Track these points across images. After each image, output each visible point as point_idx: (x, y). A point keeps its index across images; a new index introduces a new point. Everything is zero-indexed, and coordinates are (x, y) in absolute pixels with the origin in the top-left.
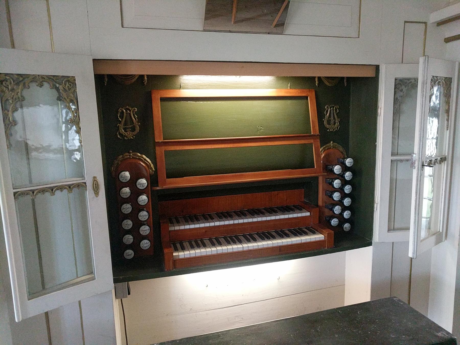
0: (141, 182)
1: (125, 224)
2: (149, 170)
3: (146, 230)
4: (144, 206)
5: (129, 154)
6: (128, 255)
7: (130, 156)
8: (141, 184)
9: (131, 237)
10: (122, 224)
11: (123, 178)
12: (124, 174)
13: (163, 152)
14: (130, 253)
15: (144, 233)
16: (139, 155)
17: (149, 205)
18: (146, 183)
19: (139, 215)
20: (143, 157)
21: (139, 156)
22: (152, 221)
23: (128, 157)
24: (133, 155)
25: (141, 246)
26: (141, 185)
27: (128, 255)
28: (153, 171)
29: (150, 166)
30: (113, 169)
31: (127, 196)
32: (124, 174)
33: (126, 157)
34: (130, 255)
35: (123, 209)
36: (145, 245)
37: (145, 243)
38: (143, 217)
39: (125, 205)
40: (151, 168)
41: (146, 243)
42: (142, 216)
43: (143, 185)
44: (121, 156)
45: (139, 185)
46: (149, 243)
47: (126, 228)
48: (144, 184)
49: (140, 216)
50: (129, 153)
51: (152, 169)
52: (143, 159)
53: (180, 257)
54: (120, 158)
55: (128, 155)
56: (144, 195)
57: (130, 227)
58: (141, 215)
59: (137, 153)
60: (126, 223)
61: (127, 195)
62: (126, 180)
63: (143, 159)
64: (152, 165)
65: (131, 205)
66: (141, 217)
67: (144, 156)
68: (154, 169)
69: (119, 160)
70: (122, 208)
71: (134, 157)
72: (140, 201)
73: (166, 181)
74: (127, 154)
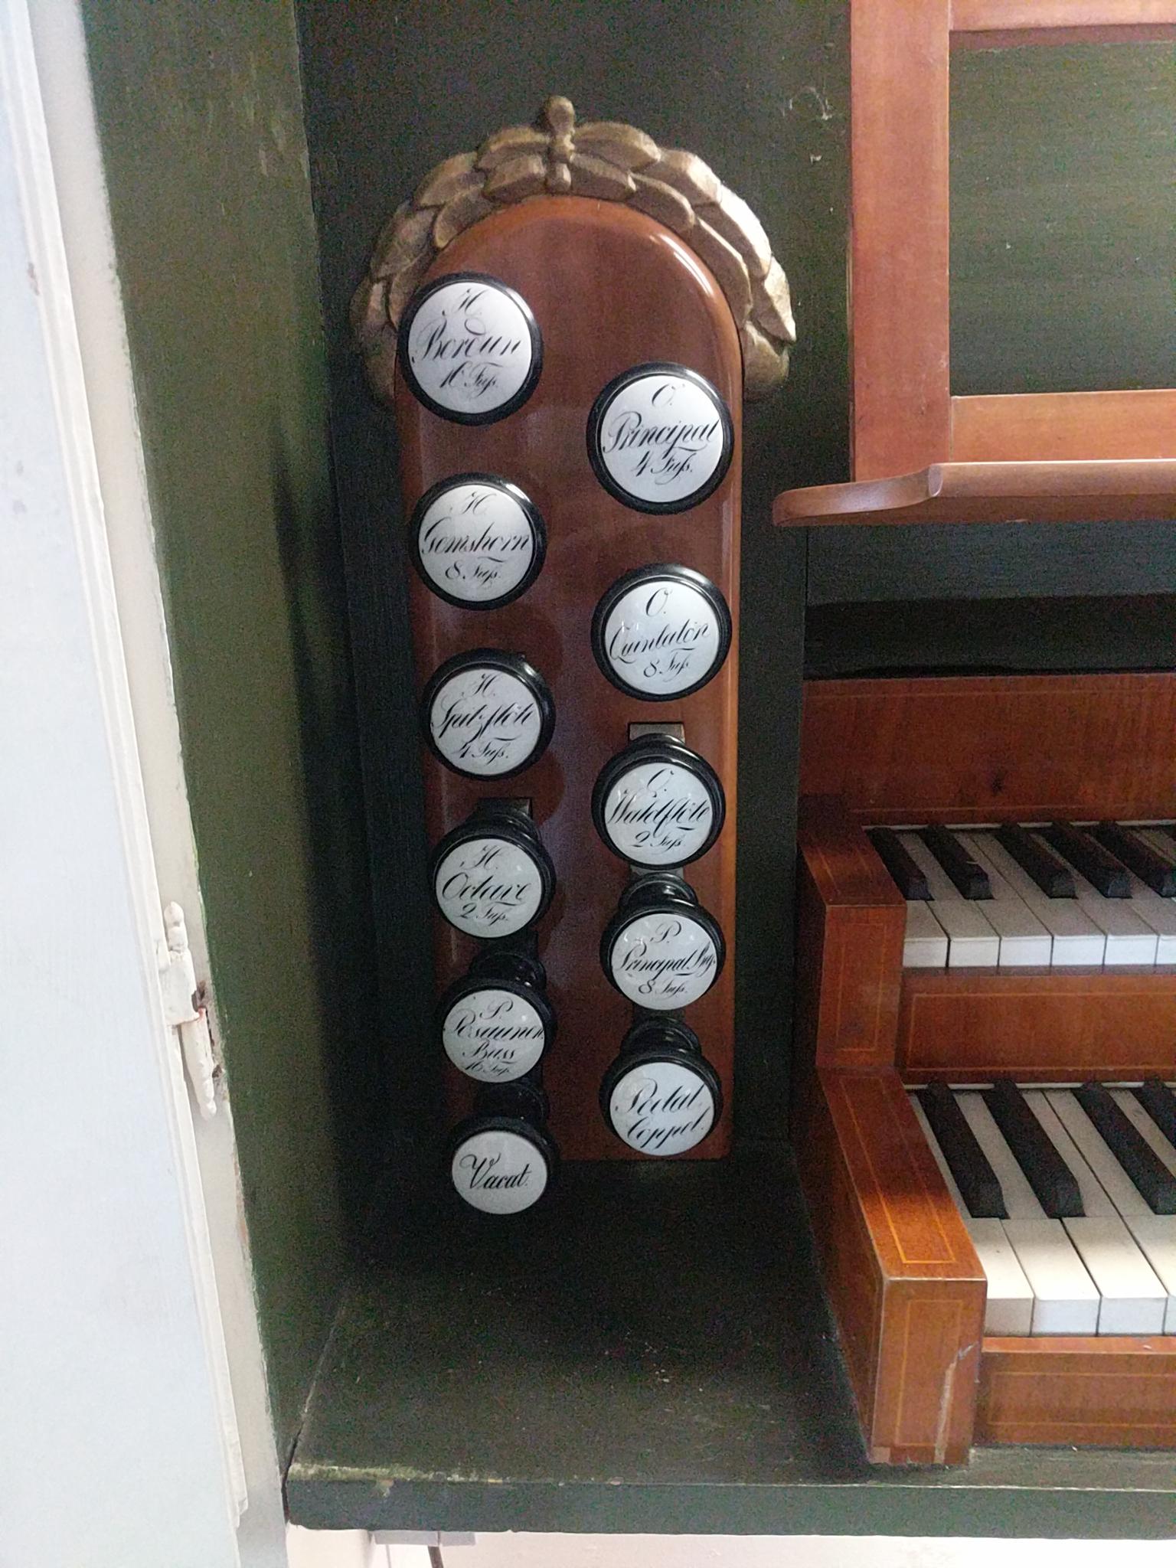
0: (659, 416)
1: (460, 880)
2: (740, 331)
3: (672, 965)
4: (674, 709)
5: (540, 138)
6: (492, 1183)
7: (551, 156)
8: (651, 436)
9: (524, 1014)
10: (441, 881)
11: (448, 364)
12: (467, 303)
13: (940, 47)
14: (507, 1167)
15: (660, 986)
16: (653, 150)
17: (720, 692)
18: (707, 431)
19: (616, 795)
20: (684, 184)
21: (645, 166)
22: (730, 868)
23: (536, 167)
24: (584, 146)
25: (615, 1117)
26: (657, 449)
27: (492, 1183)
28: (779, 342)
29: (758, 279)
30: (375, 301)
31: (489, 577)
32: (467, 303)
33: (508, 175)
34: (513, 1181)
35: (451, 719)
36: (661, 1120)
37: (663, 1095)
38: (650, 824)
39: (474, 676)
40: (765, 314)
41: (672, 1101)
42: (645, 815)
43: (679, 456)
44: (460, 164)
45: (636, 453)
46: (706, 1099)
47: (479, 925)
48: (685, 433)
49: (451, 719)
50: (542, 122)
51: (774, 314)
52: (686, 203)
53: (1045, 1326)
54: (451, 186)
55: (530, 149)
56: (677, 578)
57: (520, 913)
58: (639, 805)
59: (633, 130)
60: (479, 875)
61: (489, 566)
62: (484, 383)
63: (686, 203)
64: (776, 282)
65: (540, 691)
66: (639, 826)
67: (699, 171)
68: (791, 327)
69: (438, 208)
70: (438, 715)
71: (597, 167)
72: (626, 649)
73: (943, 425)
74: (528, 136)
